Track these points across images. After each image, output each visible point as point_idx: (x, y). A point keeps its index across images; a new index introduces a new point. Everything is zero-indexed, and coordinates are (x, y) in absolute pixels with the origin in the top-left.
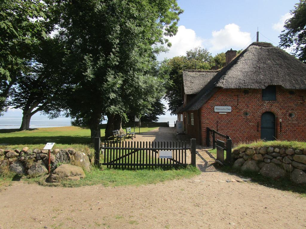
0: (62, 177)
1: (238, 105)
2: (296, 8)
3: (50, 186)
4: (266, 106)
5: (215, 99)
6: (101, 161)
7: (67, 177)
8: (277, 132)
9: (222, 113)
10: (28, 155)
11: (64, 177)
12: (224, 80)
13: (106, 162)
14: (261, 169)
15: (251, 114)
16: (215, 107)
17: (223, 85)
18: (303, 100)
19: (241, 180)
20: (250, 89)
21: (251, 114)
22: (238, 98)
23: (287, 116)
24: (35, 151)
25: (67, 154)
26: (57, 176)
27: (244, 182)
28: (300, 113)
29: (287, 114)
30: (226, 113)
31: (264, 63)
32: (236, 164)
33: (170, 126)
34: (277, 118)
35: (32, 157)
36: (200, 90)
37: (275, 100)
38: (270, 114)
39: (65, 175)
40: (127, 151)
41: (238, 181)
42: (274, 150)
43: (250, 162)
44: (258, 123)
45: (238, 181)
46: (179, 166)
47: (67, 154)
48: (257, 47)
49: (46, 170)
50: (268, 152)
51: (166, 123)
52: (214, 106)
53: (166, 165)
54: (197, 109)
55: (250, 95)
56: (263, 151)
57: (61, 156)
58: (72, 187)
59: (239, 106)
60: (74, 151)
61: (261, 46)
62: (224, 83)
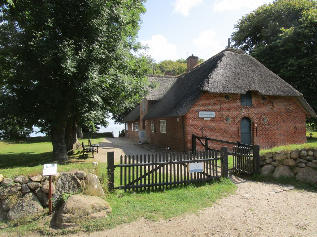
0: (81, 217)
1: (220, 110)
2: (238, 24)
3: (63, 233)
4: (245, 112)
5: (199, 104)
6: (117, 184)
7: (88, 215)
8: (253, 137)
9: (206, 119)
10: (6, 188)
11: (84, 215)
12: (209, 84)
13: (123, 185)
14: (296, 174)
15: (232, 119)
16: (200, 113)
17: (209, 89)
18: (273, 106)
19: (286, 188)
20: (230, 94)
21: (232, 119)
22: (220, 103)
23: (261, 121)
24: (19, 179)
25: (73, 178)
26: (72, 215)
27: (290, 190)
28: (270, 117)
29: (261, 119)
30: (210, 119)
31: (241, 69)
32: (266, 170)
33: (114, 136)
34: (254, 122)
35: (14, 189)
36: (163, 95)
37: (252, 105)
38: (247, 119)
39: (85, 212)
40: (151, 166)
41: (284, 190)
42: (299, 154)
43: (282, 167)
44: (238, 128)
45: (284, 190)
46: (210, 180)
47: (73, 178)
48: (232, 53)
49: (40, 208)
50: (301, 156)
51: (110, 133)
52: (199, 112)
53: (197, 180)
54: (183, 115)
55: (230, 100)
56: (296, 155)
57: (64, 184)
58: (102, 230)
59: (221, 111)
60: (85, 174)
61: (235, 52)
62: (210, 87)
